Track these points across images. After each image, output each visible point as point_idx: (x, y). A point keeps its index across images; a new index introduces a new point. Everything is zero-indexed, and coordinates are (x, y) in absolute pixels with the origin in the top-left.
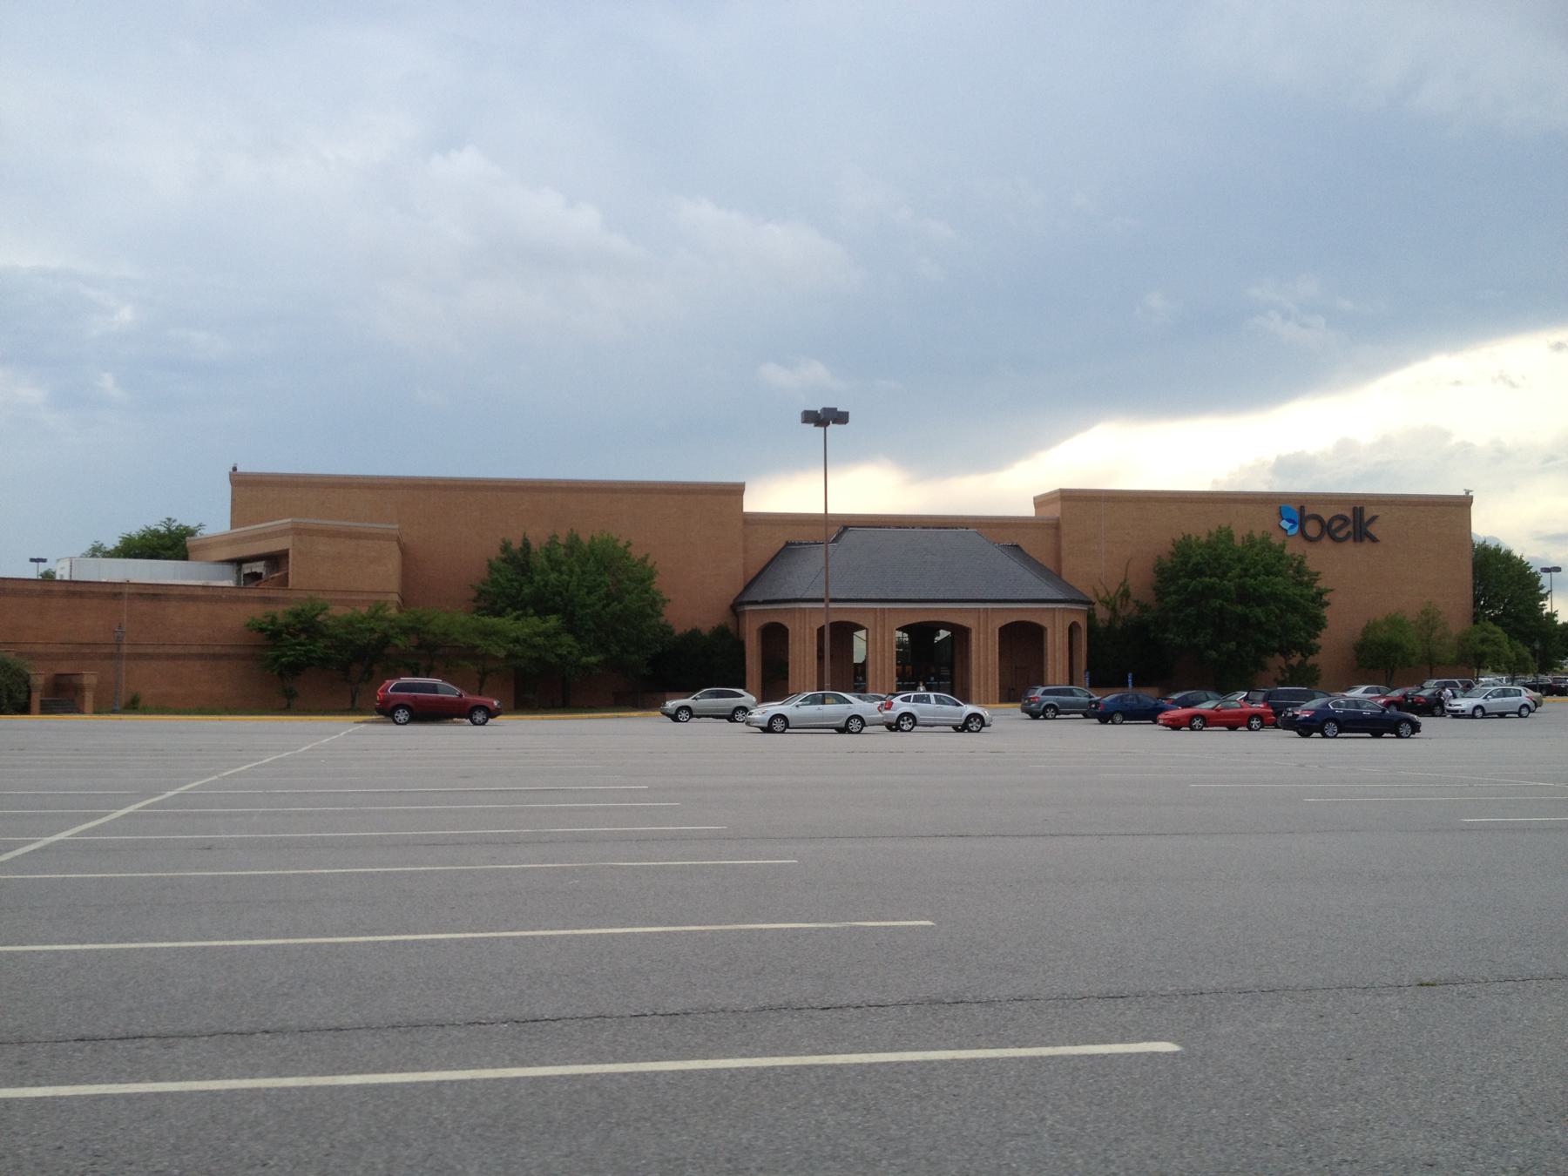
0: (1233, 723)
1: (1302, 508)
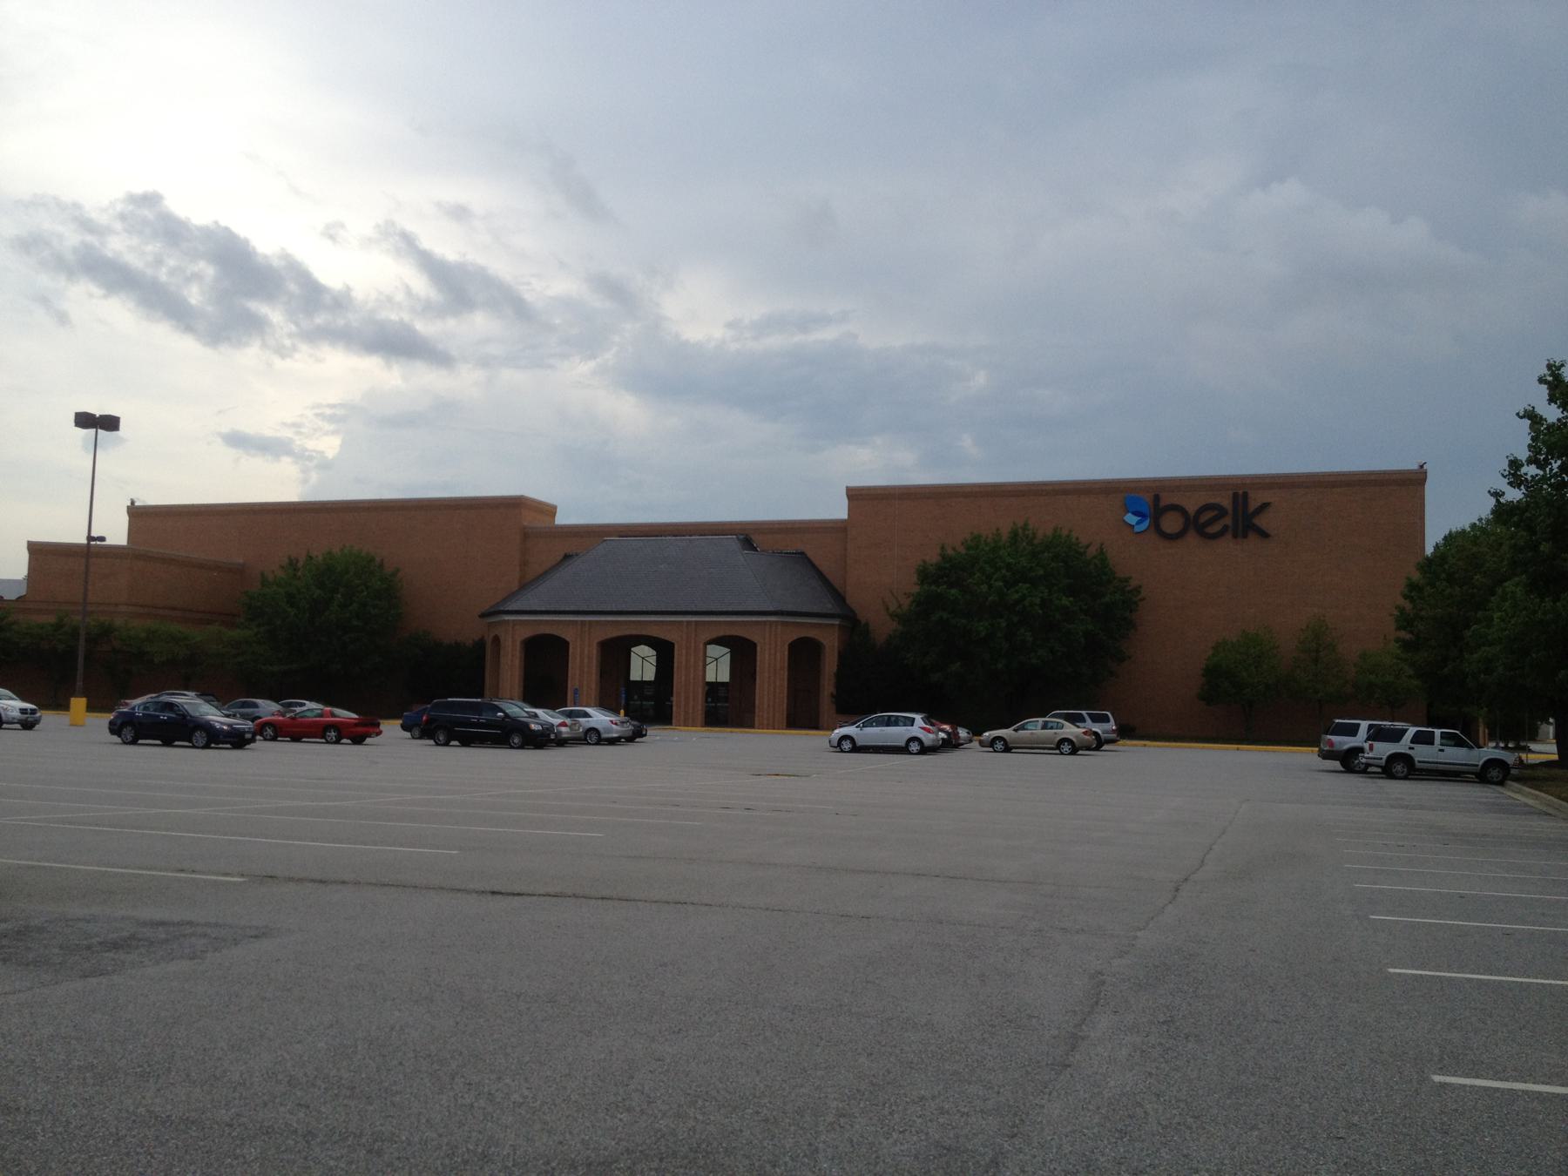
0: (295, 732)
1: (1157, 498)
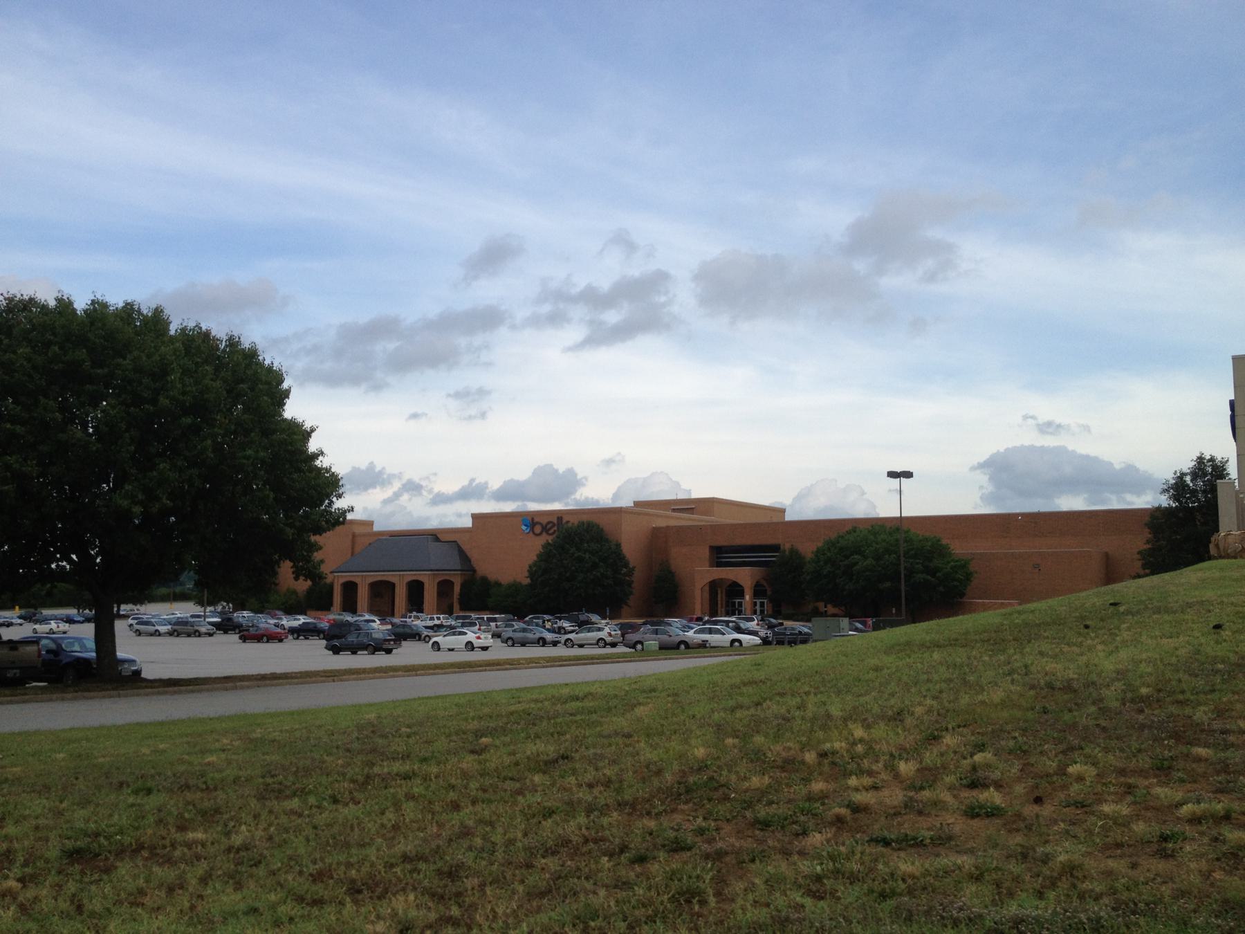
1: (533, 519)
